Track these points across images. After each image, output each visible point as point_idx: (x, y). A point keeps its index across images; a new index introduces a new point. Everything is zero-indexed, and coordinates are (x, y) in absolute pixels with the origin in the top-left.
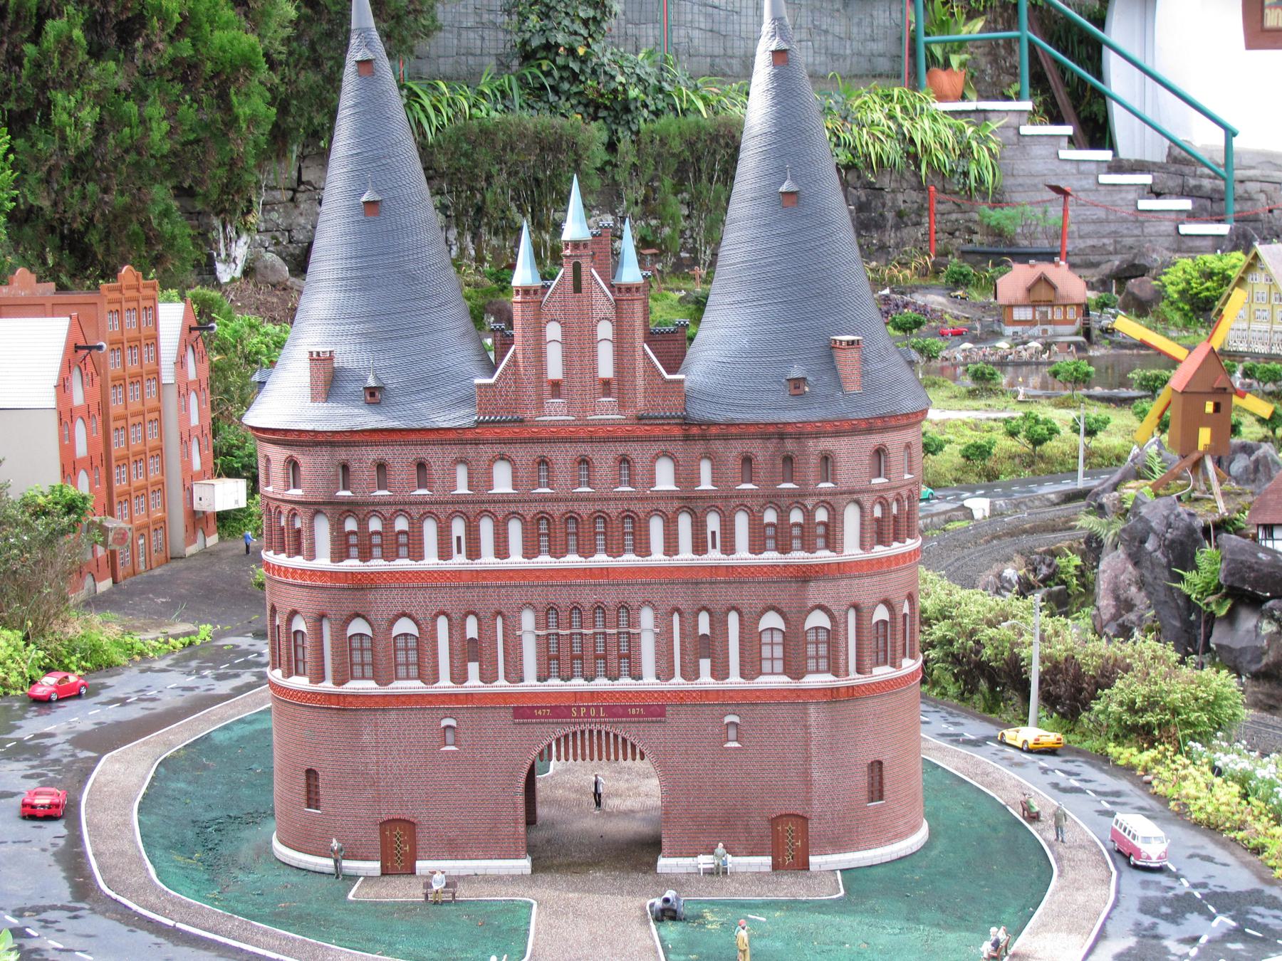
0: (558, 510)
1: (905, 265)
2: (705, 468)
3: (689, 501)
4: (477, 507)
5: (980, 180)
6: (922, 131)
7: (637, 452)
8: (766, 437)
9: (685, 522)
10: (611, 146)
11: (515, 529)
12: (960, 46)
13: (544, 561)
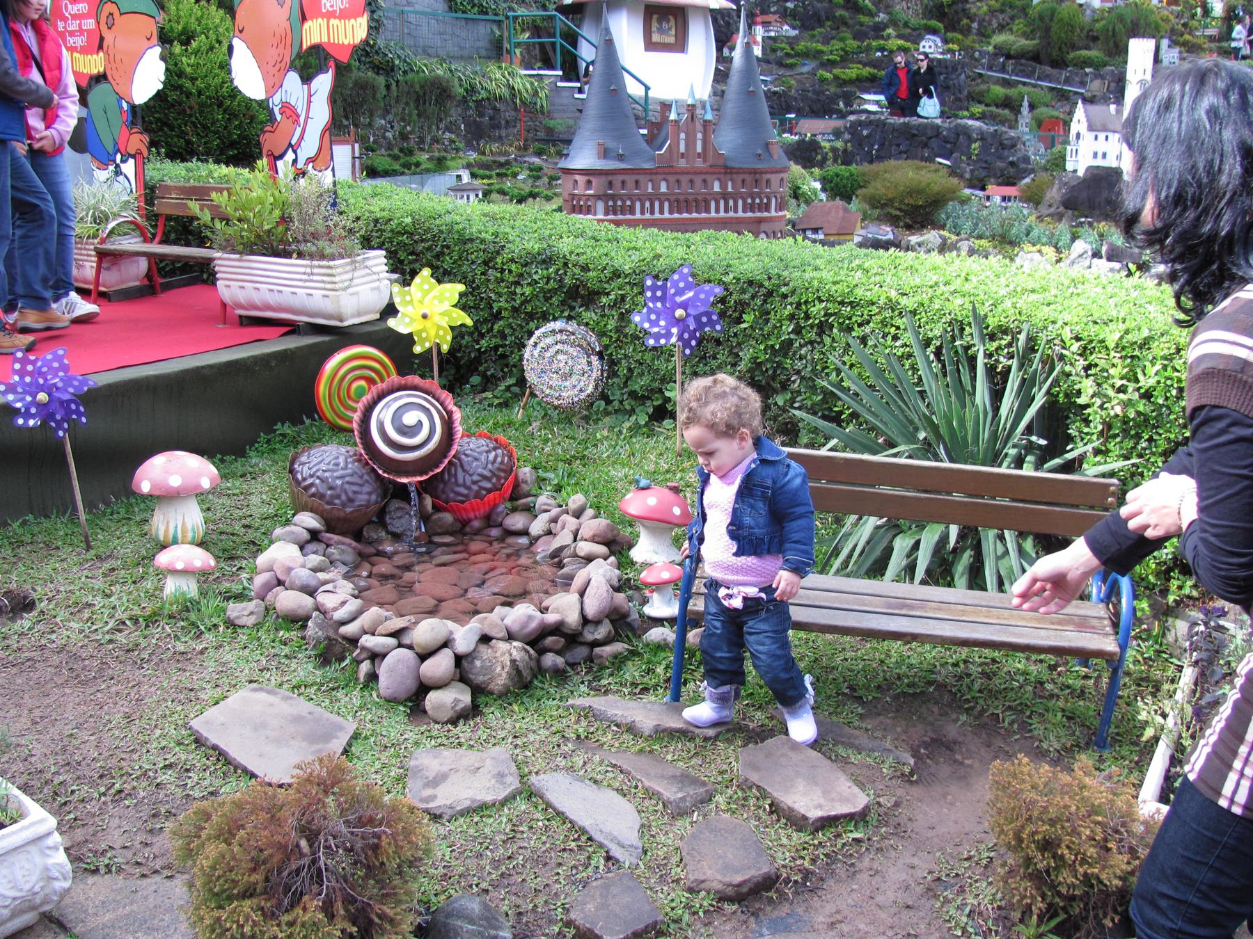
0: (682, 198)
1: (511, 145)
2: (730, 184)
3: (725, 196)
4: (656, 197)
5: (542, 106)
6: (518, 84)
7: (709, 178)
8: (750, 173)
9: (722, 203)
10: (388, 87)
11: (666, 205)
12: (518, 45)
13: (676, 216)
